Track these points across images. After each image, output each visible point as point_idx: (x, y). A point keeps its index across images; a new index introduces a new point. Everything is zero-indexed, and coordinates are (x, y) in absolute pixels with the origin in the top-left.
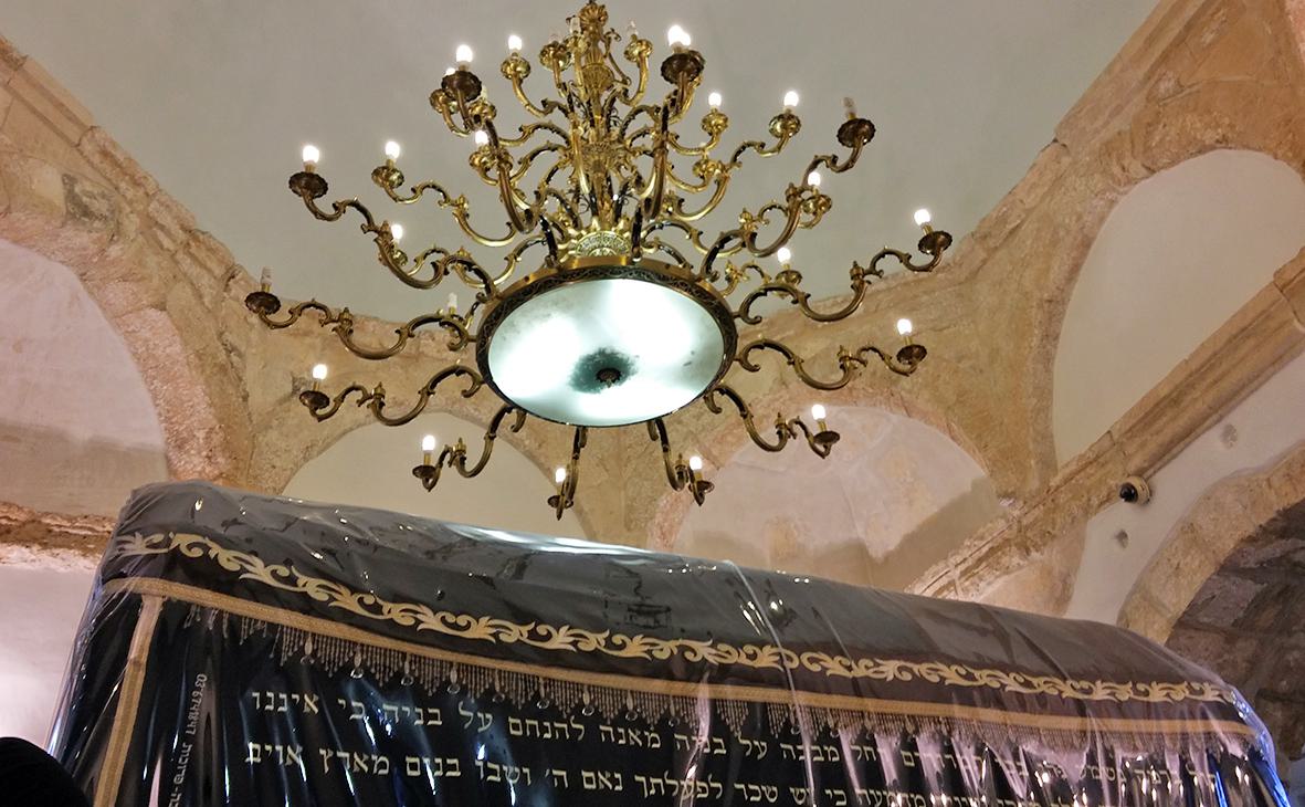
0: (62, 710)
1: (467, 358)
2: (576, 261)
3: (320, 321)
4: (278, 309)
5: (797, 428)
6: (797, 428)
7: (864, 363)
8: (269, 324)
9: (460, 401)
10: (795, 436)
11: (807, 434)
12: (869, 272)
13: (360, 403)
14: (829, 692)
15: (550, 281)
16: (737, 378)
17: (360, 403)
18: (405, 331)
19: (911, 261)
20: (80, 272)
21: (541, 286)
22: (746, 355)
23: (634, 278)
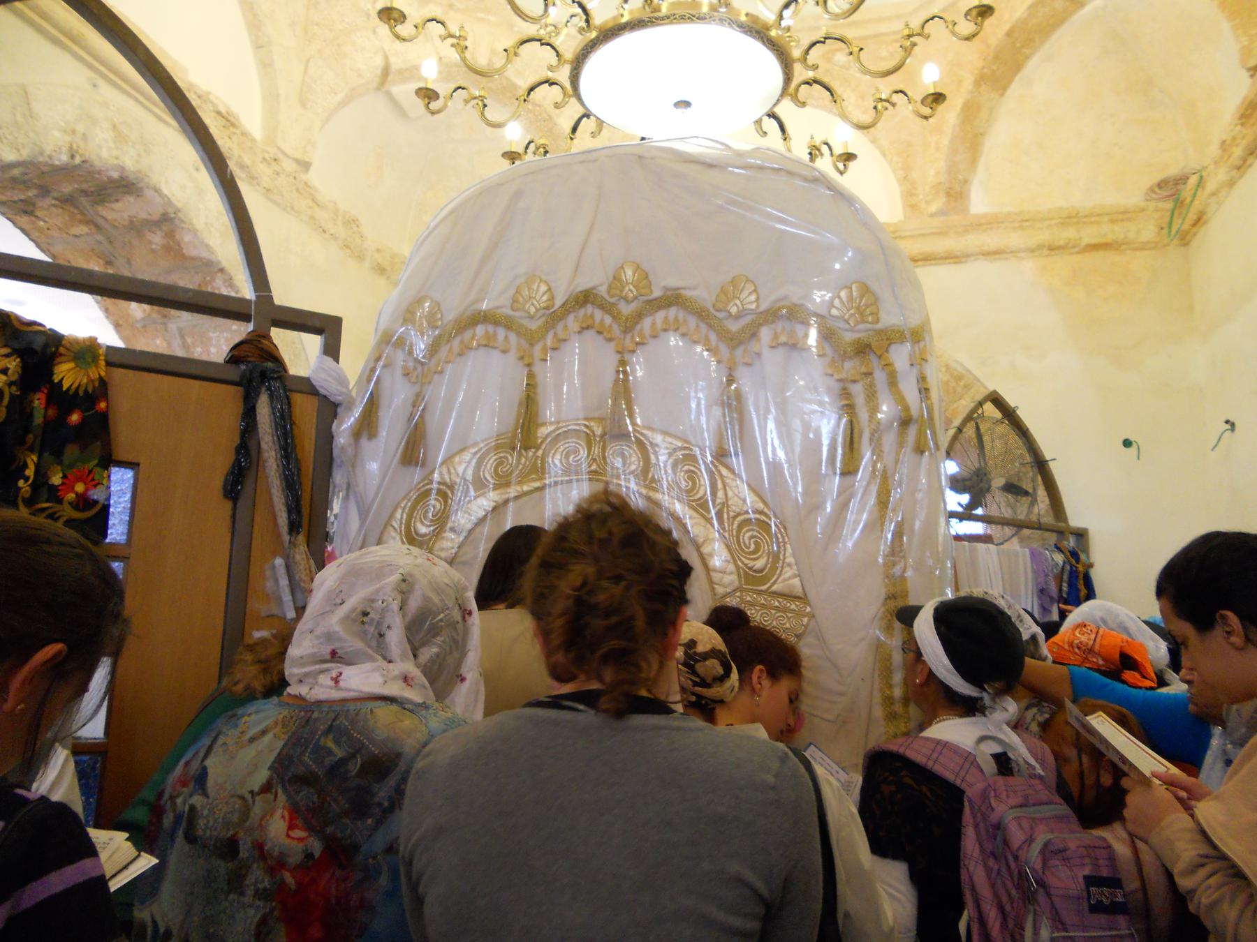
0: (472, 190)
1: (563, 75)
2: (344, 721)
3: (440, 36)
4: (403, 22)
5: (825, 149)
6: (825, 149)
7: (894, 105)
8: (398, 37)
9: (368, 16)
10: (822, 155)
11: (832, 154)
12: (918, 35)
13: (467, 102)
14: (1247, 742)
15: (644, 21)
16: (786, 110)
17: (467, 102)
18: (511, 51)
19: (956, 28)
20: (605, 132)
21: (634, 25)
22: (797, 90)
23: (717, 24)
